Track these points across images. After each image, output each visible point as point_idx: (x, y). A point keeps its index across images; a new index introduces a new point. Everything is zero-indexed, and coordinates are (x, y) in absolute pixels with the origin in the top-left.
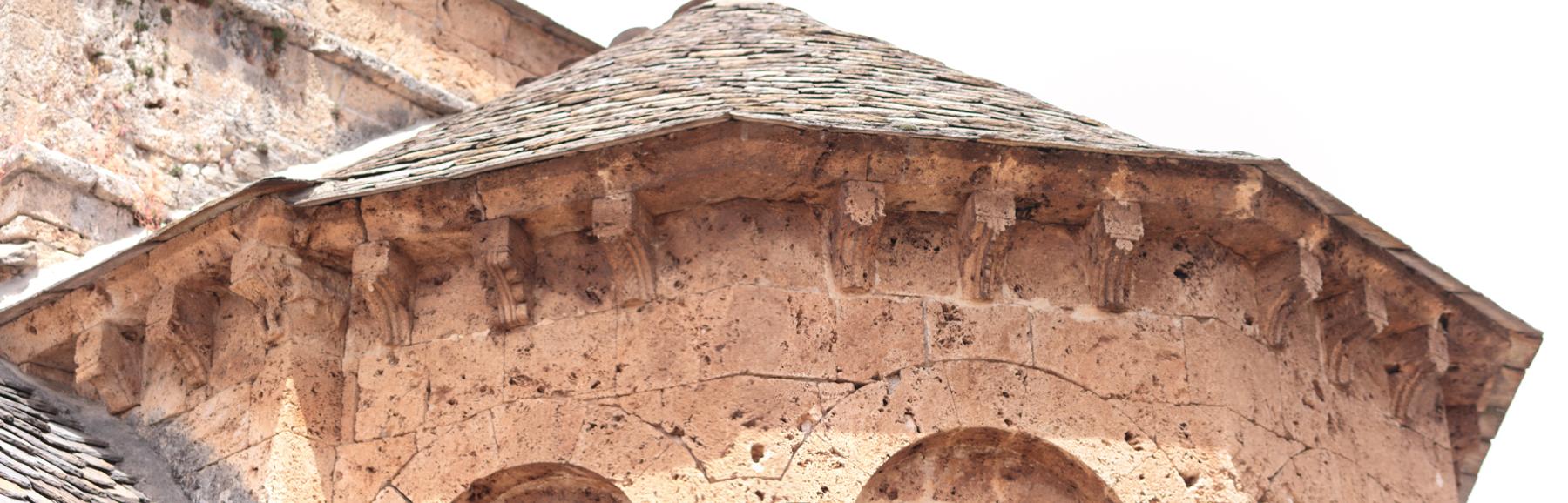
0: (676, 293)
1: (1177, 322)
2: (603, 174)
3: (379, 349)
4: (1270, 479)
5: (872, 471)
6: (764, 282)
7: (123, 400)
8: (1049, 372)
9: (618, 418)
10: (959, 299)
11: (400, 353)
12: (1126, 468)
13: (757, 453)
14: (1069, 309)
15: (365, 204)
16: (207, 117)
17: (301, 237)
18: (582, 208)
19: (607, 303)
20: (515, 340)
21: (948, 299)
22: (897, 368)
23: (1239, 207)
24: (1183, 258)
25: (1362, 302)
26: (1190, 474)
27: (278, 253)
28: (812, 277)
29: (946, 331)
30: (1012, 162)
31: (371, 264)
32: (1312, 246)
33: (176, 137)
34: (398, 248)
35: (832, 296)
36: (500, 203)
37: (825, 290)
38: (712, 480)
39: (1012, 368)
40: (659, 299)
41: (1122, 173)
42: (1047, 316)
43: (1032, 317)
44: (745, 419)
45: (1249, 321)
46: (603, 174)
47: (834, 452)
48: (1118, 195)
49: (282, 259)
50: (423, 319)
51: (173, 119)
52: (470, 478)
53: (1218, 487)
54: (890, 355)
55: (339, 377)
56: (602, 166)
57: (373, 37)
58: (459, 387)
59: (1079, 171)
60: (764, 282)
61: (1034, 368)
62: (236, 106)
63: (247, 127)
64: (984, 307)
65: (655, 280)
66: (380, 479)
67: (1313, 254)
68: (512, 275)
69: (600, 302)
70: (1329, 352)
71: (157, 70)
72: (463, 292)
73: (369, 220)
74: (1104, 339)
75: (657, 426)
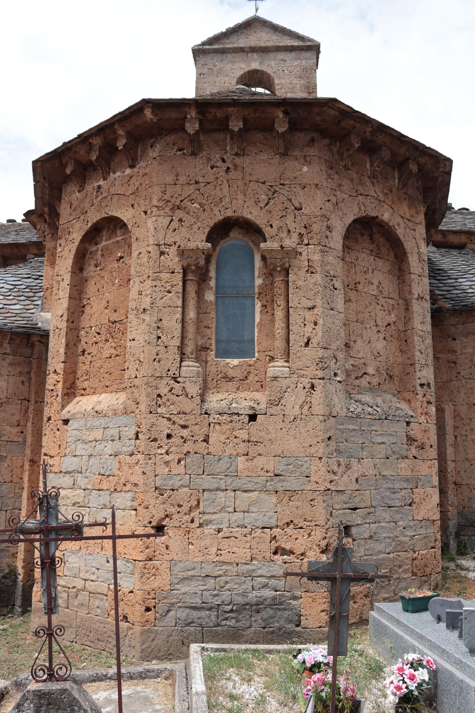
32: (194, 116)
64: (106, 182)
67: (195, 118)
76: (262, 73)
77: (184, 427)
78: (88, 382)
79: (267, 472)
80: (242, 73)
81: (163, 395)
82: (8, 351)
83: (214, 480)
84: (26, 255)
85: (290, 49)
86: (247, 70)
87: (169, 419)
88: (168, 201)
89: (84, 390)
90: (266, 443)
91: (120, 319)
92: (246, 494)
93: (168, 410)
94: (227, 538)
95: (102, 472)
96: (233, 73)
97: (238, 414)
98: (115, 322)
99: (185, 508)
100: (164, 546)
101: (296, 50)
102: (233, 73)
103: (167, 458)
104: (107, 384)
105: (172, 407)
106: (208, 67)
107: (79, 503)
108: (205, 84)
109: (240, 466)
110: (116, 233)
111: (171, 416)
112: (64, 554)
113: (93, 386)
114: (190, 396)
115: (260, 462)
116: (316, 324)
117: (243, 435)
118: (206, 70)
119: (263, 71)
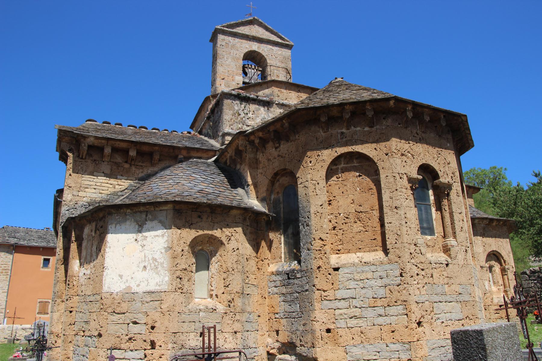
0: (298, 138)
1: (384, 127)
2: (284, 121)
3: (261, 154)
4: (404, 152)
5: (330, 162)
6: (310, 134)
7: (234, 167)
8: (360, 140)
9: (292, 160)
10: (344, 130)
11: (264, 154)
12: (375, 154)
13: (311, 162)
14: (364, 128)
15: (255, 132)
16: (258, 118)
17: (247, 139)
18: (282, 126)
19: (290, 141)
20: (278, 150)
21: (342, 131)
22: (333, 144)
23: (391, 105)
24: (384, 115)
25: (423, 117)
26: (387, 153)
27: (244, 142)
28: (319, 131)
29: (342, 136)
30: (348, 106)
31: (257, 141)
32: (410, 109)
33: (253, 123)
34: (260, 138)
35: (322, 134)
36: (272, 128)
37: (321, 133)
38: (304, 168)
39: (354, 141)
40: (296, 139)
41: (368, 104)
42: (360, 130)
43: (357, 131)
44: (308, 157)
45: (399, 124)
46: (284, 121)
47: (323, 160)
48: (369, 107)
49: (245, 143)
50: (267, 148)
51: (252, 120)
52: (274, 173)
53: (392, 155)
54: (332, 142)
55: (257, 160)
56: (283, 120)
57: (286, 99)
58: (272, 158)
59: (360, 105)
60: (310, 134)
61: (358, 140)
62: (263, 116)
63: (265, 118)
64: (348, 131)
65: (295, 136)
66: (263, 174)
67: (410, 110)
68: (275, 139)
69: (288, 141)
70: (419, 127)
71: (248, 113)
72: (270, 144)
73: (256, 135)
74: (371, 132)
75: (297, 160)
76: (258, 54)
77: (423, 270)
78: (342, 246)
79: (456, 292)
80: (247, 51)
81: (412, 253)
82: (249, 224)
83: (437, 297)
84: (177, 156)
85: (276, 43)
86: (249, 50)
87: (416, 266)
88: (399, 151)
89: (339, 251)
90: (454, 278)
91: (366, 211)
92: (450, 303)
93: (415, 261)
94: (446, 326)
95: (375, 296)
96: (241, 49)
97: (442, 264)
98: (361, 212)
99: (429, 312)
100: (423, 332)
101: (279, 45)
102: (241, 49)
103: (419, 286)
104: (360, 247)
105: (416, 259)
106: (225, 41)
107: (356, 316)
108: (224, 53)
109: (446, 290)
110: (353, 161)
111: (417, 264)
112: (346, 348)
113: (347, 248)
114: (423, 254)
115: (453, 287)
116: (463, 220)
117: (445, 274)
118: (224, 43)
119: (259, 53)
